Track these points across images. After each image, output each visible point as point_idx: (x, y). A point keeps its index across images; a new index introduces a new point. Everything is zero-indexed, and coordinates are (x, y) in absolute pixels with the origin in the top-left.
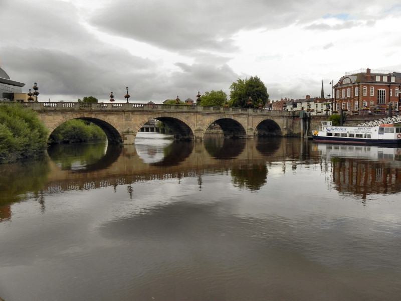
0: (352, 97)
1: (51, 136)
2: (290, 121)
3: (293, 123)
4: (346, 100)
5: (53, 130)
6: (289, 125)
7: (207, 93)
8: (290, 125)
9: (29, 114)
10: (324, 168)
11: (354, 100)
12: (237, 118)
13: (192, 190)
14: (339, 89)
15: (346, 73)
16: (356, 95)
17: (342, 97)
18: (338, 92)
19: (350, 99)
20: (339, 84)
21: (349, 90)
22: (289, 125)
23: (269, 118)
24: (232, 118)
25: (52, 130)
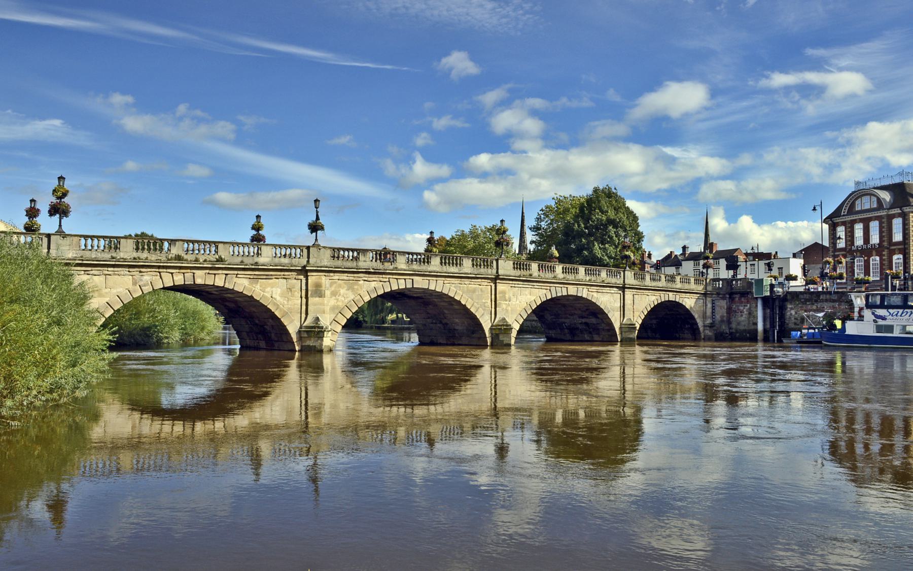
0: (885, 244)
1: (714, 384)
2: (723, 304)
3: (729, 310)
4: (866, 252)
5: (231, 287)
6: (718, 317)
7: (643, 241)
8: (722, 317)
9: (38, 509)
10: (594, 363)
11: (892, 253)
12: (595, 294)
13: (636, 470)
14: (844, 223)
15: (858, 183)
16: (898, 237)
17: (853, 244)
18: (841, 231)
19: (879, 250)
20: (844, 211)
21: (874, 226)
22: (718, 317)
23: (672, 297)
24: (584, 293)
25: (640, 322)
